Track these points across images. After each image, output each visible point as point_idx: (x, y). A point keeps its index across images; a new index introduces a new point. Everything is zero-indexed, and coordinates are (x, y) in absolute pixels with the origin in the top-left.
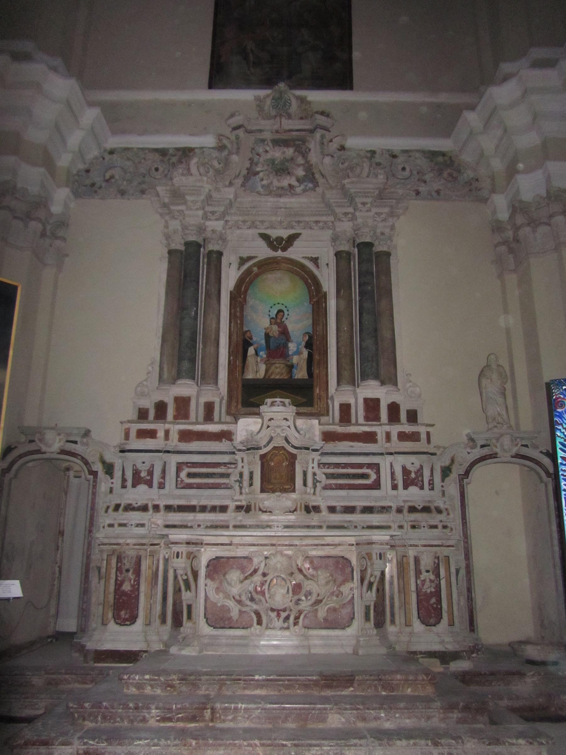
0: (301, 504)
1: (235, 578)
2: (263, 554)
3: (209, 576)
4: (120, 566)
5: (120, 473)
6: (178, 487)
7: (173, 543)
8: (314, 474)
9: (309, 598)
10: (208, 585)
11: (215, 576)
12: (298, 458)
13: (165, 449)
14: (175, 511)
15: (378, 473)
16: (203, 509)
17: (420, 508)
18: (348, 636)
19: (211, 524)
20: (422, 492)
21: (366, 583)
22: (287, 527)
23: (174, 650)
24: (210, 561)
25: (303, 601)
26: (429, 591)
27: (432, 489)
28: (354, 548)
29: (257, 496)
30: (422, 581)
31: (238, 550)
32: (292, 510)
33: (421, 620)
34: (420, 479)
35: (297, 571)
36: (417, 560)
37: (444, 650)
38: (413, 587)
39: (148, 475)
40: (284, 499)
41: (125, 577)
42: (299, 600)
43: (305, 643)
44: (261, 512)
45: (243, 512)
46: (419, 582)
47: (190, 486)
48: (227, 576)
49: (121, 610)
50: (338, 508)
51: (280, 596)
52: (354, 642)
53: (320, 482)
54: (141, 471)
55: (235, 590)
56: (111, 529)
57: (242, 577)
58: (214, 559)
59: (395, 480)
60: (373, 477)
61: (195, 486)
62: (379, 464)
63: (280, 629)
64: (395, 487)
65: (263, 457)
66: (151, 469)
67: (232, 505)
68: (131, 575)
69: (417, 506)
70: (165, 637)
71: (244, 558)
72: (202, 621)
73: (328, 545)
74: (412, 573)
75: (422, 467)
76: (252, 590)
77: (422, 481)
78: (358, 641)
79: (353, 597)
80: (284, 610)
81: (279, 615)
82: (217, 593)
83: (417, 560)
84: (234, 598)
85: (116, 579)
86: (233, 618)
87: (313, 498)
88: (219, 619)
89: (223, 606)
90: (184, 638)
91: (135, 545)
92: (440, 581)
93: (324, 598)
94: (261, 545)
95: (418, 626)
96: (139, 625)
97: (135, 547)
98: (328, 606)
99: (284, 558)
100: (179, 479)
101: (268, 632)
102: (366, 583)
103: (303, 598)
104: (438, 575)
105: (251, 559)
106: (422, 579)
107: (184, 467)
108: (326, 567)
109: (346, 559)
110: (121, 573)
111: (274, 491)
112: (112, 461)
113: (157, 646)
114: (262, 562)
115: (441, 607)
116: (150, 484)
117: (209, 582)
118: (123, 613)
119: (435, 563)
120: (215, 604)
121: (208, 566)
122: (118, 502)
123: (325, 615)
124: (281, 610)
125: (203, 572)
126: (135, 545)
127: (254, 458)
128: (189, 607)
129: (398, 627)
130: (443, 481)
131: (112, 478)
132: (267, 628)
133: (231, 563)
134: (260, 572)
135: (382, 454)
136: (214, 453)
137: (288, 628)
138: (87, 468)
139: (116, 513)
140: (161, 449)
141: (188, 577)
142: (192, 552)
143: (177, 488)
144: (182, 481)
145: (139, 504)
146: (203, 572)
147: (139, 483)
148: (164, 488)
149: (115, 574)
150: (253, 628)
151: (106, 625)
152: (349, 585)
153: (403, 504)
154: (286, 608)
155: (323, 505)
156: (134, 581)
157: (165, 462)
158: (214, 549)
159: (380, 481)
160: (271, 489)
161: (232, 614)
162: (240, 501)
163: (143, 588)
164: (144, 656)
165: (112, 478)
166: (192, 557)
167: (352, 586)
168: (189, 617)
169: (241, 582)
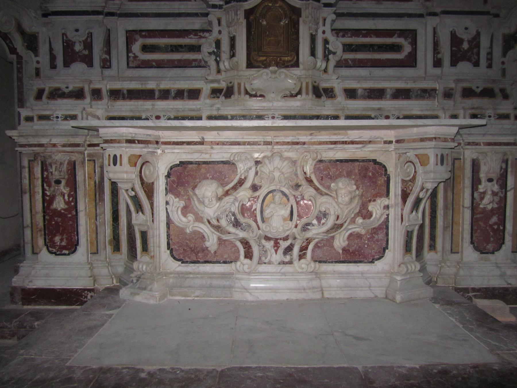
0: (307, 84)
1: (209, 194)
2: (252, 157)
3: (170, 190)
4: (47, 176)
5: (47, 46)
6: (130, 65)
7: (106, 141)
8: (326, 42)
9: (323, 221)
10: (171, 203)
11: (181, 190)
12: (303, 14)
13: (106, 11)
14: (124, 98)
15: (414, 43)
16: (165, 95)
17: (478, 91)
18: (378, 273)
19: (176, 114)
20: (476, 70)
21: (411, 200)
22: (286, 117)
23: (124, 293)
24: (171, 168)
25: (313, 225)
26: (489, 207)
27: (490, 66)
28: (392, 147)
29: (241, 73)
30: (481, 193)
31: (214, 151)
32: (294, 92)
33: (474, 247)
34: (475, 51)
35: (304, 182)
36: (475, 166)
37: (506, 286)
38: (467, 202)
39: (85, 48)
40: (283, 76)
41: (54, 191)
42: (308, 224)
43: (316, 283)
44: (248, 96)
45: (222, 98)
46: (476, 195)
47: (146, 65)
48: (197, 191)
49: (55, 236)
50: (360, 92)
51: (278, 220)
52: (386, 281)
53: (334, 53)
54: (75, 42)
55: (210, 211)
56: (29, 124)
57: (220, 191)
58: (177, 165)
59: (438, 53)
60: (408, 49)
61: (154, 64)
62: (415, 31)
63: (279, 264)
64: (438, 63)
65: (248, 13)
66: (89, 40)
67: (206, 88)
68: (63, 188)
69: (474, 88)
70: (120, 270)
71: (223, 162)
72: (165, 254)
73: (352, 143)
74: (468, 182)
75: (478, 34)
76: (237, 212)
77: (478, 54)
78: (392, 280)
79: (387, 219)
80: (286, 239)
81: (277, 245)
82: (184, 214)
83: (475, 166)
84: (209, 222)
85: (44, 194)
86: (209, 249)
87: (325, 76)
88: (188, 249)
89: (195, 232)
90: (139, 278)
91: (64, 146)
92: (506, 194)
93: (345, 222)
94: (249, 143)
95: (469, 254)
96: (81, 254)
97: (65, 149)
98: (350, 232)
99: (286, 163)
100: (130, 55)
101: (262, 268)
102: (411, 200)
103: (315, 222)
104: (503, 185)
105: (233, 164)
106: (481, 190)
107: (137, 37)
108: (349, 175)
109: (380, 164)
110: (49, 186)
111: (266, 66)
112: (34, 30)
113: (105, 283)
114: (250, 168)
115: (504, 227)
116: (89, 61)
117: (171, 197)
118: (57, 239)
119: (501, 168)
120: (182, 231)
121: (168, 176)
122: (42, 86)
123: (345, 244)
124: (281, 239)
125: (161, 185)
126: (64, 146)
127: (236, 14)
128: (144, 235)
129: (439, 254)
130: (504, 55)
131: (36, 55)
132: (260, 262)
133: (203, 171)
134: (248, 184)
135: (421, 16)
136: (179, 15)
137: (291, 263)
138: (8, 46)
139: (39, 103)
140: (100, 9)
141: (136, 193)
142: (140, 156)
143: (128, 67)
144: (135, 57)
145: (71, 88)
146: (161, 185)
147: (73, 61)
148: (110, 67)
149: (40, 188)
150: (238, 263)
151: (37, 254)
152: (383, 201)
153: (453, 86)
154: (288, 236)
155: (338, 86)
156: (69, 196)
157: (109, 30)
158: (177, 149)
159: (416, 55)
160: (262, 62)
161: (208, 244)
162: (218, 81)
163: (83, 205)
164: (89, 297)
165: (36, 55)
166: (140, 163)
167: (386, 203)
168: (145, 248)
169: (219, 199)
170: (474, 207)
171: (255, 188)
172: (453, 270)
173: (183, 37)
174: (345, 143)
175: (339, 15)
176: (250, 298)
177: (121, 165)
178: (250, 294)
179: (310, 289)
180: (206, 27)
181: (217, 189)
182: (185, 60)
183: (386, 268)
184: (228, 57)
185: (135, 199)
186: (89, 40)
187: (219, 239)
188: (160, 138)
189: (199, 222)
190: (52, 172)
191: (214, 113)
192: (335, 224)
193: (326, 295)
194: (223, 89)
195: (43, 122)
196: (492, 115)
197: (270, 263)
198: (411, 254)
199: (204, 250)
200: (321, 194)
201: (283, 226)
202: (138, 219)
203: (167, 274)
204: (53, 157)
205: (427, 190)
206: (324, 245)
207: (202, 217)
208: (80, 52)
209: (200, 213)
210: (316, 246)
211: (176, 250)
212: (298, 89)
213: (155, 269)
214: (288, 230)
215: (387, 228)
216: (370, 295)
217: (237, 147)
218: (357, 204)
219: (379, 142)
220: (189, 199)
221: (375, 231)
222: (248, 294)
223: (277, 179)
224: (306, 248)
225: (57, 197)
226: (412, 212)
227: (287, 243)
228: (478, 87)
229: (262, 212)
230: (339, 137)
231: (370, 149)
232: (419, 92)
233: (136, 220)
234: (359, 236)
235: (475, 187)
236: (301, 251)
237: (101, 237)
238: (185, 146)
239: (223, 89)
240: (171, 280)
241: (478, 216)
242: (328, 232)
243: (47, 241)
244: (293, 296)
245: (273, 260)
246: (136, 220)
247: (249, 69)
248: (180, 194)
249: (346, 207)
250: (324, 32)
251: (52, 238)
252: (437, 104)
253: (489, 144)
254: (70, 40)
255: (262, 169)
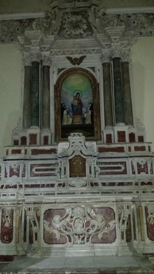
0: (89, 182)
3: (45, 218)
5: (4, 170)
6: (32, 176)
8: (95, 168)
9: (94, 228)
11: (48, 218)
12: (87, 160)
14: (30, 187)
15: (125, 166)
17: (146, 183)
18: (113, 247)
21: (121, 220)
24: (46, 211)
25: (91, 230)
29: (68, 179)
30: (149, 218)
33: (149, 238)
34: (146, 168)
36: (146, 209)
38: (145, 222)
40: (81, 180)
42: (89, 229)
43: (92, 250)
44: (70, 187)
45: (62, 187)
46: (147, 219)
47: (37, 175)
49: (5, 236)
50: (107, 184)
51: (79, 228)
52: (116, 250)
53: (98, 171)
55: (57, 226)
57: (61, 219)
59: (134, 169)
60: (123, 168)
64: (134, 173)
65: (70, 160)
66: (19, 168)
67: (57, 184)
68: (9, 219)
69: (145, 182)
72: (42, 241)
73: (102, 202)
74: (144, 215)
75: (147, 163)
79: (115, 227)
80: (82, 235)
81: (79, 237)
83: (146, 209)
84: (57, 229)
87: (95, 179)
90: (34, 249)
93: (101, 228)
98: (103, 232)
101: (75, 245)
102: (121, 220)
107: (34, 166)
109: (112, 209)
110: (4, 218)
111: (76, 177)
113: (21, 253)
114: (70, 211)
116: (18, 175)
117: (45, 221)
121: (44, 214)
122: (3, 184)
124: (80, 235)
125: (42, 217)
128: (36, 234)
129: (138, 241)
133: (55, 212)
134: (70, 216)
135: (127, 157)
137: (84, 243)
141: (35, 220)
142: (37, 208)
143: (31, 176)
144: (33, 173)
145: (13, 185)
146: (42, 217)
150: (67, 244)
153: (138, 181)
156: (10, 222)
158: (48, 205)
159: (126, 170)
161: (57, 237)
162: (60, 181)
164: (15, 258)
167: (114, 222)
168: (36, 239)
169: (60, 221)
170: (147, 224)
171: (72, 217)
172: (142, 247)
173: (49, 166)
174: (100, 202)
175: (99, 158)
176: (70, 256)
177: (31, 211)
178: (71, 254)
179: (90, 252)
180: (56, 163)
181: (60, 218)
182: (50, 174)
183: (116, 245)
184: (64, 174)
185: (34, 222)
186: (19, 168)
187: (61, 235)
188: (42, 202)
189: (54, 229)
190: (6, 214)
191: (59, 192)
192: (97, 229)
193: (96, 255)
194: (62, 184)
195: (4, 197)
196: (150, 191)
197: (77, 243)
198: (124, 240)
199: (55, 239)
200: (93, 219)
201: (81, 230)
202: (34, 229)
203: (43, 248)
204: (7, 208)
205: (126, 217)
206: (95, 237)
207: (55, 228)
208: (15, 172)
209: (54, 226)
210: (92, 237)
211: (46, 239)
212: (86, 184)
213: (39, 246)
214: (82, 231)
215: (115, 231)
216: (111, 255)
217: (66, 204)
218: (105, 222)
219: (110, 202)
220: (51, 222)
221: (112, 231)
222: (70, 255)
223: (79, 214)
224: (89, 238)
225: (7, 222)
226: (122, 225)
227: (83, 236)
228: (146, 182)
229: (74, 225)
230: (98, 200)
231: (108, 204)
232: (127, 183)
233: (34, 229)
234: (106, 234)
235: (147, 216)
236: (87, 239)
237: (20, 237)
238: (50, 204)
239: (62, 184)
240: (44, 250)
241: (149, 227)
242: (95, 232)
243: (2, 238)
244: (85, 255)
245: (78, 242)
246: (34, 229)
247: (70, 178)
248: (48, 220)
249: (100, 223)
250: (94, 165)
251: (3, 237)
252: (133, 187)
253: (150, 201)
254: (12, 168)
255: (74, 211)
